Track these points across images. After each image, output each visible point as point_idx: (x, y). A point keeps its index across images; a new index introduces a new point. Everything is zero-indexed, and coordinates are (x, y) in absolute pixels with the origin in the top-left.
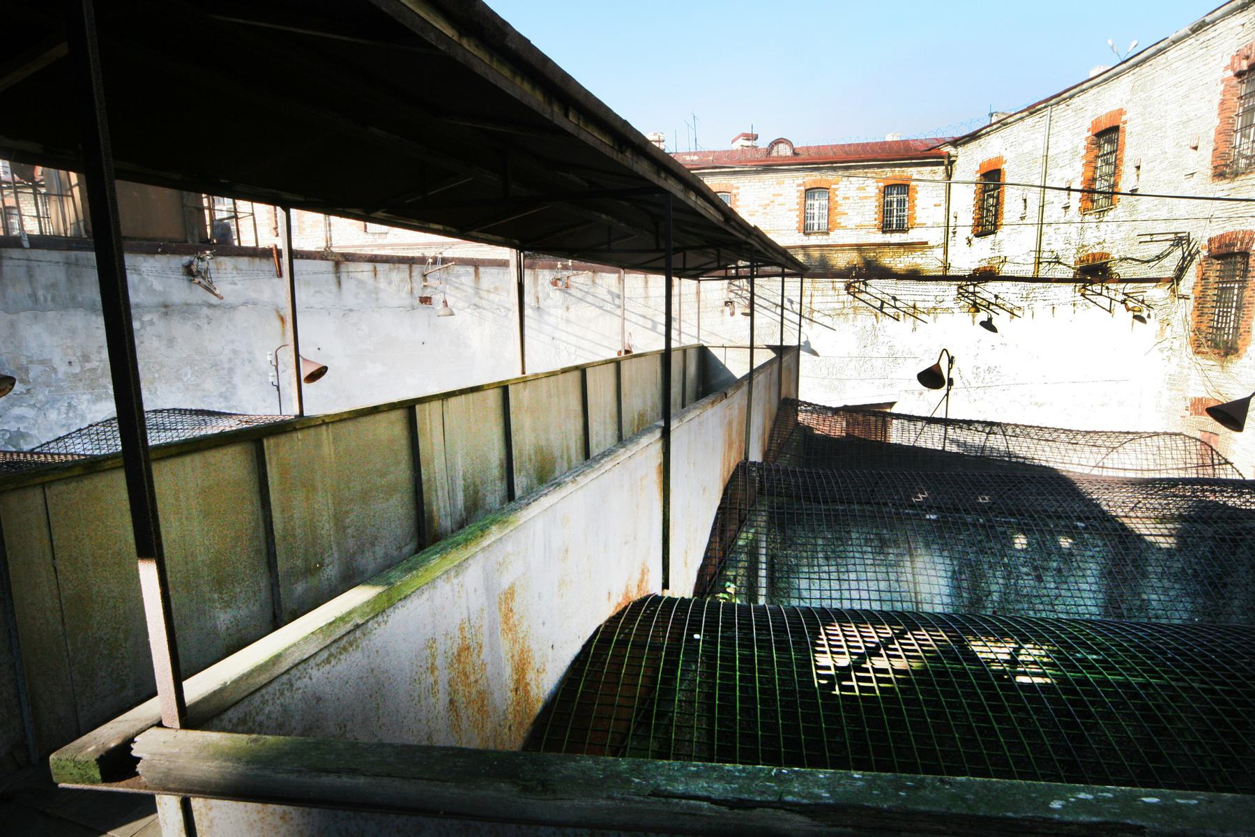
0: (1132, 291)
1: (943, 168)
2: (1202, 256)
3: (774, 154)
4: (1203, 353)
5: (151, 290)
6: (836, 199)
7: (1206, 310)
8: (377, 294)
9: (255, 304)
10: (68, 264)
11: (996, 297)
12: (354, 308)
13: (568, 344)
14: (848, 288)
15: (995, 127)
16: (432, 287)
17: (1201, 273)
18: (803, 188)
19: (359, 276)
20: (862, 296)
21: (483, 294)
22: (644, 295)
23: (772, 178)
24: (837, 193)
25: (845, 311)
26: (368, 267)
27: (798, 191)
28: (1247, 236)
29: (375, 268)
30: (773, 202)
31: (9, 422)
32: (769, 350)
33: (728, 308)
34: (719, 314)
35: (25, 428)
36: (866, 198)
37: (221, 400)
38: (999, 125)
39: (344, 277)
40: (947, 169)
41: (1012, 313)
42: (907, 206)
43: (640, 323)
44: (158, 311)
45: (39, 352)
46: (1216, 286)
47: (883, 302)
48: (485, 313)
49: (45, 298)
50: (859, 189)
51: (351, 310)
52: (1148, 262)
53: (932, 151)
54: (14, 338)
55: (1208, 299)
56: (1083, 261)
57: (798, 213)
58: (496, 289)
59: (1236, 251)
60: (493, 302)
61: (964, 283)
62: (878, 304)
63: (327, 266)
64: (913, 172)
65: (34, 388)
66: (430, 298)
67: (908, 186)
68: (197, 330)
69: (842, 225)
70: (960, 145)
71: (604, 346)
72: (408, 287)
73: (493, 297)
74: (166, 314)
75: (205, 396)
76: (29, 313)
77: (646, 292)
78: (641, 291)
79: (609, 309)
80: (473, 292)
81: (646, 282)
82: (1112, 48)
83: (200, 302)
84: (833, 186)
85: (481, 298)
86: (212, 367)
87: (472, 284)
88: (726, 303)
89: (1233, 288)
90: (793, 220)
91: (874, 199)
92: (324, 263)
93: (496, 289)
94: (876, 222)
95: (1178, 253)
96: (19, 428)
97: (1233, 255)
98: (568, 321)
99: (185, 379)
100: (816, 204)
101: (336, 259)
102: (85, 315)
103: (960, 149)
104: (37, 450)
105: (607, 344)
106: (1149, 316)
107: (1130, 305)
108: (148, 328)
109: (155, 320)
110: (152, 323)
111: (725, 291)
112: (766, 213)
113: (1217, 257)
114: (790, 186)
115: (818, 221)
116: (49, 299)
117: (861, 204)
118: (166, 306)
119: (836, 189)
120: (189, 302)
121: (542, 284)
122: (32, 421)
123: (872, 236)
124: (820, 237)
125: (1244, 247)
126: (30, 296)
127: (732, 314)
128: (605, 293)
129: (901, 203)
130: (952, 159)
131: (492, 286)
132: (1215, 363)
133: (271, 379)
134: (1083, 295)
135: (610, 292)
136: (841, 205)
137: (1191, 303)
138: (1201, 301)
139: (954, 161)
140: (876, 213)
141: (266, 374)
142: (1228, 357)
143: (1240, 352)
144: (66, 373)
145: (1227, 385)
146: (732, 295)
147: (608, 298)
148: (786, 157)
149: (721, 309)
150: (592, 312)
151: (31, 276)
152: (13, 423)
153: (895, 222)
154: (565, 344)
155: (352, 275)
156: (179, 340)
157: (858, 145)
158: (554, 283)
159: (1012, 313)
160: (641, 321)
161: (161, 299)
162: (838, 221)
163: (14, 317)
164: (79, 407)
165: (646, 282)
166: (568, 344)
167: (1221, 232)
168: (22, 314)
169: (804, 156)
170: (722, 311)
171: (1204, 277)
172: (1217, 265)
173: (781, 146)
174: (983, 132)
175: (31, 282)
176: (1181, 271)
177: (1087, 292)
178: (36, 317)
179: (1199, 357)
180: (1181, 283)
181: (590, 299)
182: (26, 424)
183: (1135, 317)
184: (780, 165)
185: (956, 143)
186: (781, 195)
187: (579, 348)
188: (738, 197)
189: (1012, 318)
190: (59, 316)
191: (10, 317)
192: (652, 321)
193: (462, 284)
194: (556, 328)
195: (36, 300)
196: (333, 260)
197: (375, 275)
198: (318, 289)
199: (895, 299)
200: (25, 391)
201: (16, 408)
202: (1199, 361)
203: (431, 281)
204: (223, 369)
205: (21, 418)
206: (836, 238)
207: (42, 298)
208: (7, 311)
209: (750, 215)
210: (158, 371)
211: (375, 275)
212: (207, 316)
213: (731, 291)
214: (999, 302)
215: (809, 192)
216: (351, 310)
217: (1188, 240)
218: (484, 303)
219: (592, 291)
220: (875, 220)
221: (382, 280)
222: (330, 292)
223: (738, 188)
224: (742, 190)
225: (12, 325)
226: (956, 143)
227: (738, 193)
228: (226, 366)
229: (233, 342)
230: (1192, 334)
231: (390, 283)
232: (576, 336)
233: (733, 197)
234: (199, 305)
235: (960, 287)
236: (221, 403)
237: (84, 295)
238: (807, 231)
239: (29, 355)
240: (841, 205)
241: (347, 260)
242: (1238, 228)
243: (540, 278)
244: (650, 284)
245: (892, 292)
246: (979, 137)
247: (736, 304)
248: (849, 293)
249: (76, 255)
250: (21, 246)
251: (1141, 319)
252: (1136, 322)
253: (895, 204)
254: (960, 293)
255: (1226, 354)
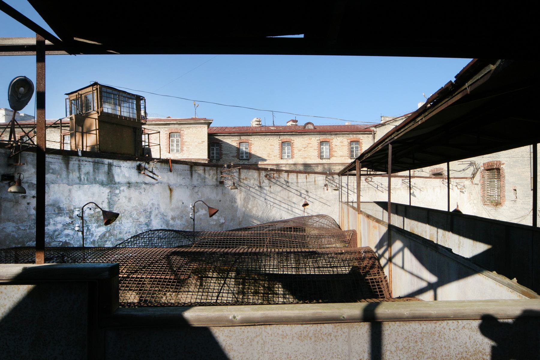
0: (459, 182)
1: (371, 135)
2: (481, 170)
3: (307, 128)
4: (487, 205)
5: (124, 176)
6: (332, 146)
7: (485, 189)
8: (205, 179)
9: (161, 183)
10: (94, 162)
11: (415, 184)
12: (196, 186)
13: (270, 201)
14: (366, 180)
15: (391, 121)
16: (224, 177)
17: (482, 176)
18: (319, 141)
19: (199, 172)
20: (371, 183)
21: (242, 180)
22: (296, 182)
23: (307, 137)
24: (332, 143)
25: (365, 189)
26: (202, 168)
27: (317, 142)
28: (498, 163)
29: (205, 168)
30: (308, 146)
31: (62, 237)
32: (375, 203)
33: (325, 188)
34: (322, 190)
35: (69, 240)
36: (343, 146)
37: (146, 226)
38: (393, 121)
39: (194, 172)
40: (373, 136)
41: (420, 190)
42: (359, 149)
43: (296, 193)
44: (126, 185)
45: (79, 204)
46: (488, 180)
47: (378, 185)
48: (242, 188)
49: (84, 179)
50: (341, 142)
51: (195, 186)
52: (460, 171)
53: (367, 129)
54: (70, 197)
55: (486, 185)
56: (432, 171)
57: (318, 151)
58: (246, 178)
59: (494, 168)
60: (245, 184)
61: (404, 178)
62: (376, 186)
63: (187, 167)
64: (361, 137)
65: (75, 221)
66: (223, 182)
67: (359, 142)
68: (140, 194)
69: (335, 155)
70: (377, 127)
71: (283, 203)
72: (215, 177)
73: (245, 182)
74: (129, 187)
75: (140, 225)
76: (77, 186)
77: (297, 181)
78: (295, 180)
79: (284, 187)
80: (238, 179)
81: (297, 176)
82: (424, 96)
83: (142, 182)
84: (331, 141)
85: (241, 182)
86: (144, 211)
87: (237, 176)
88: (325, 185)
89: (495, 181)
90: (316, 153)
91: (347, 146)
92: (187, 166)
93: (246, 178)
94: (348, 155)
95: (472, 168)
96: (66, 240)
97: (493, 169)
98: (271, 192)
99: (133, 217)
100: (324, 147)
101: (191, 164)
102: (99, 187)
103: (377, 129)
104: (118, 246)
105: (284, 202)
106: (465, 191)
107: (459, 187)
108: (122, 193)
109: (125, 190)
110: (123, 191)
111: (325, 180)
112: (305, 150)
113: (487, 170)
114: (275, 142)
115: (325, 154)
116: (86, 179)
117: (342, 148)
118: (129, 183)
119: (332, 142)
120: (137, 182)
121: (262, 177)
122: (72, 237)
123: (347, 160)
124: (327, 160)
125: (497, 166)
126: (78, 178)
127: (327, 190)
128: (283, 180)
129: (357, 148)
130: (375, 132)
131: (244, 177)
132: (491, 208)
133: (191, 216)
134: (443, 183)
135: (285, 181)
136: (334, 148)
137: (480, 187)
138: (483, 185)
139: (375, 133)
140: (348, 151)
141: (189, 214)
142: (498, 206)
143: (502, 204)
144: (88, 214)
145: (499, 217)
146: (327, 182)
147: (284, 183)
148: (311, 129)
149: (323, 187)
150: (278, 189)
151: (79, 169)
152: (64, 238)
153: (355, 155)
154: (269, 202)
155: (196, 171)
156: (133, 199)
157: (336, 126)
158: (266, 176)
159: (420, 190)
160: (296, 192)
161: (128, 180)
162: (333, 154)
163: (71, 187)
164: (92, 230)
165: (297, 176)
166: (270, 201)
167: (488, 161)
168: (75, 186)
169: (318, 129)
170: (324, 189)
171: (483, 177)
172: (487, 173)
173: (309, 125)
174: (387, 123)
175: (79, 172)
176: (474, 175)
177: (444, 182)
178: (80, 187)
179: (486, 206)
180: (474, 179)
181: (278, 183)
182: (69, 238)
183: (461, 191)
184: (310, 132)
185: (376, 126)
186: (311, 144)
187: (274, 203)
188: (294, 144)
189: (420, 192)
190: (89, 187)
191: (69, 187)
192: (300, 192)
193: (234, 176)
194: (266, 195)
195: (80, 180)
196: (190, 165)
197: (205, 171)
198: (184, 177)
199: (381, 184)
200: (71, 222)
201: (66, 230)
202: (486, 208)
203: (224, 175)
204: (148, 212)
205: (68, 235)
206: (333, 160)
207: (83, 179)
208: (69, 185)
209: (299, 151)
210: (123, 213)
211: (205, 171)
212: (144, 188)
213: (327, 181)
214: (416, 185)
215: (322, 143)
216: (195, 186)
217: (475, 164)
218: (242, 184)
219: (279, 180)
220: (348, 154)
221: (207, 174)
222: (188, 178)
223: (294, 140)
224: (295, 141)
225: (70, 191)
226: (376, 126)
227: (294, 143)
228: (149, 210)
229: (152, 200)
230: (481, 198)
231: (209, 175)
232: (273, 198)
233: (292, 144)
234: (141, 183)
235: (403, 180)
236: (145, 227)
237: (99, 178)
238: (321, 157)
239: (75, 205)
240: (334, 148)
241: (195, 165)
242: (494, 160)
243: (261, 174)
244: (299, 177)
245: (381, 182)
246: (385, 125)
247: (328, 186)
248: (366, 182)
249: (98, 160)
250: (78, 155)
251: (463, 192)
252: (461, 193)
253: (354, 148)
254: (403, 182)
255: (497, 205)
